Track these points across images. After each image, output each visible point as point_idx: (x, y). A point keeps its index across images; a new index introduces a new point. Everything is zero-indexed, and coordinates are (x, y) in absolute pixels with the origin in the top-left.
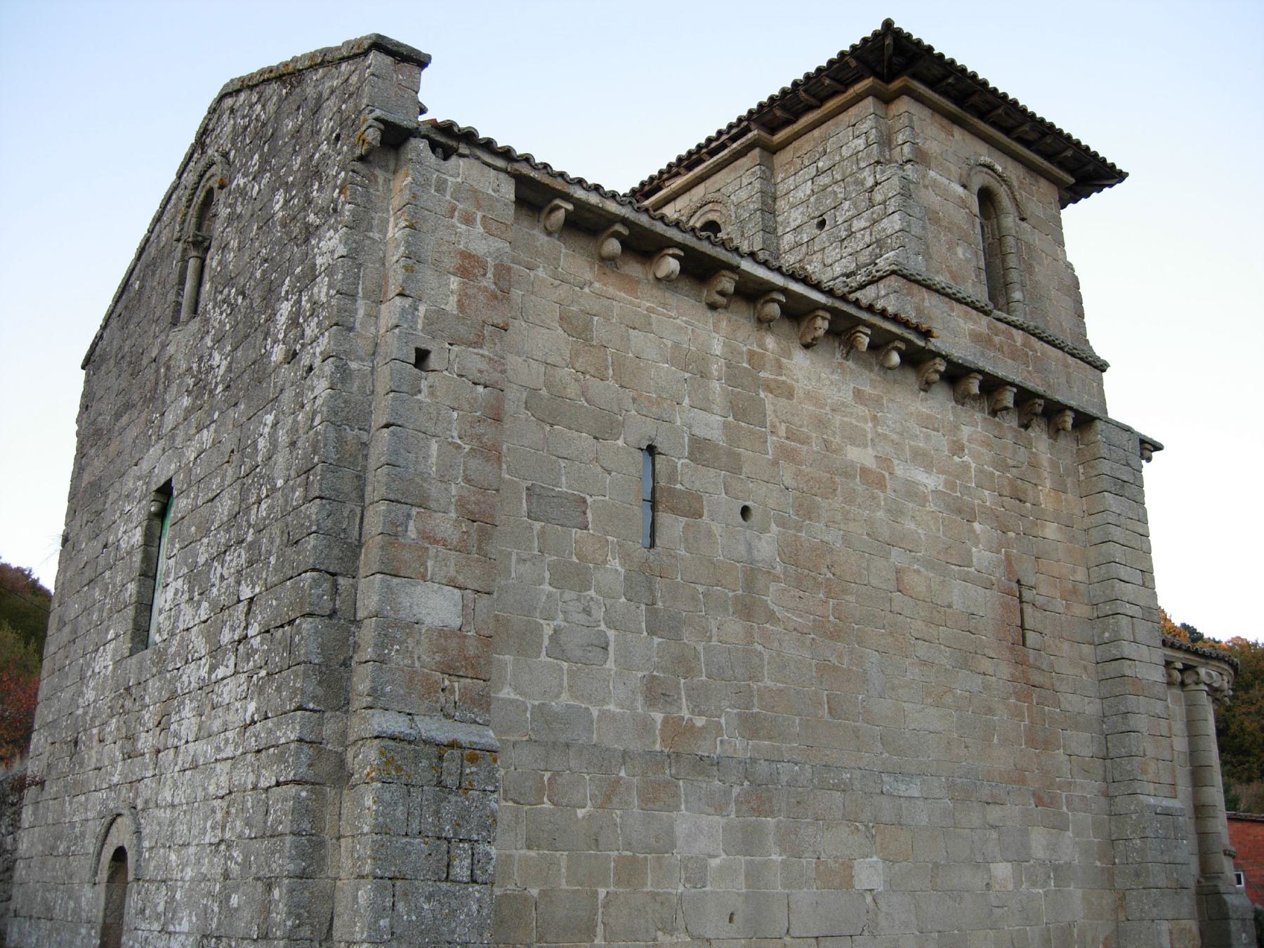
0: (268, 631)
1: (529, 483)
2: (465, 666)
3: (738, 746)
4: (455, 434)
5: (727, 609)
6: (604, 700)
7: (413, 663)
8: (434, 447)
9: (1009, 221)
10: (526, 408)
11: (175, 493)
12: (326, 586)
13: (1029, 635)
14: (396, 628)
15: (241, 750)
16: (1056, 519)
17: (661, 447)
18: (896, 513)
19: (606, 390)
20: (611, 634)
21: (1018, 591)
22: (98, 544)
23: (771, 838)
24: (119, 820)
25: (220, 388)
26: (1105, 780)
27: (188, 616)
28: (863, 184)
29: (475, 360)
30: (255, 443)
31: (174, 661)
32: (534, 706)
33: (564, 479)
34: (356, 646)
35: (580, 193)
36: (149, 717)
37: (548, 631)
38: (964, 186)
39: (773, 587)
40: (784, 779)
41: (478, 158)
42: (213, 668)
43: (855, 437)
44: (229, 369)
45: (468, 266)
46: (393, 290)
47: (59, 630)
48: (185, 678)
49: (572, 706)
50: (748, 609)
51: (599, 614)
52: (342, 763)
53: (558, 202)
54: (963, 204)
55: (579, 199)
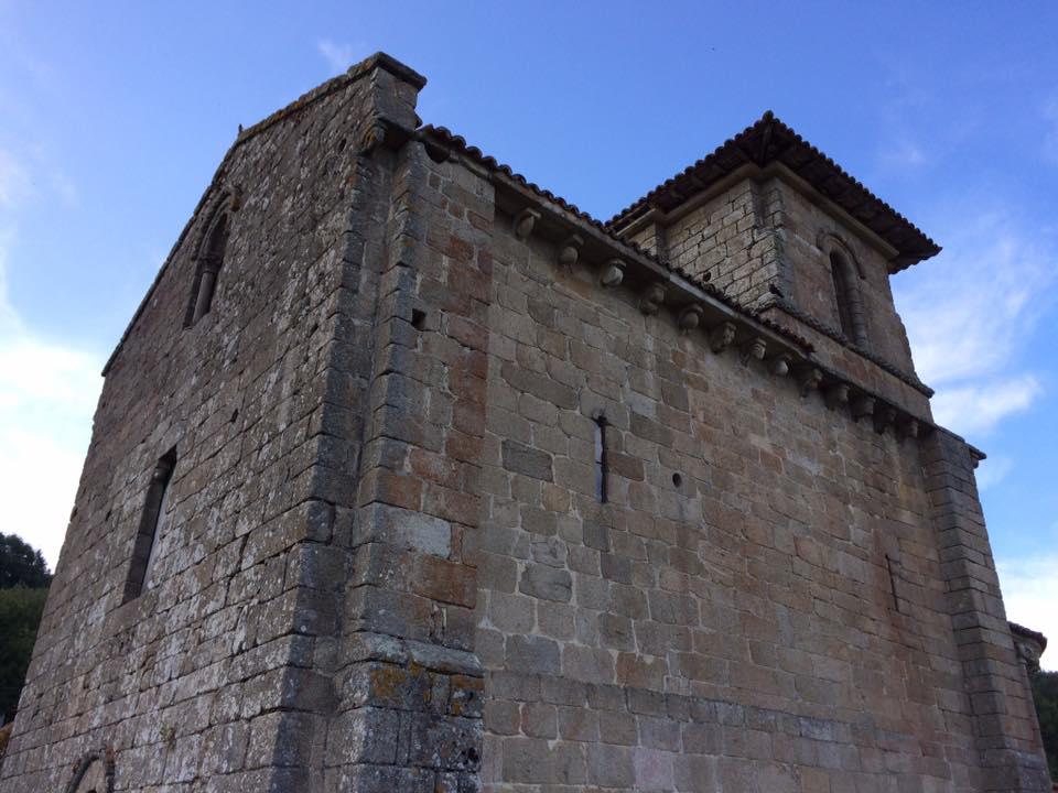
0: (262, 562)
1: (504, 439)
2: (454, 585)
3: (681, 685)
4: (446, 385)
5: (666, 561)
6: (568, 635)
7: (405, 587)
8: (427, 393)
9: (854, 278)
10: (502, 376)
11: (179, 456)
12: (325, 514)
13: (901, 602)
14: (389, 552)
15: (225, 681)
16: (910, 508)
17: (610, 418)
18: (790, 491)
19: (565, 368)
20: (573, 574)
21: (887, 565)
22: (102, 513)
23: (714, 775)
24: (94, 764)
25: (227, 362)
26: (973, 735)
27: (183, 560)
28: (742, 244)
29: (463, 326)
30: (258, 400)
31: (164, 603)
32: (509, 638)
33: (532, 438)
34: (352, 572)
35: (547, 204)
36: (134, 659)
37: (521, 568)
38: (820, 248)
39: (701, 544)
40: (721, 717)
41: (465, 165)
42: (203, 604)
43: (755, 428)
44: (237, 346)
45: (458, 249)
46: (394, 259)
47: (60, 591)
48: (174, 618)
49: (542, 639)
50: (682, 561)
51: (563, 556)
52: (331, 688)
53: (529, 210)
54: (820, 262)
55: (547, 209)
